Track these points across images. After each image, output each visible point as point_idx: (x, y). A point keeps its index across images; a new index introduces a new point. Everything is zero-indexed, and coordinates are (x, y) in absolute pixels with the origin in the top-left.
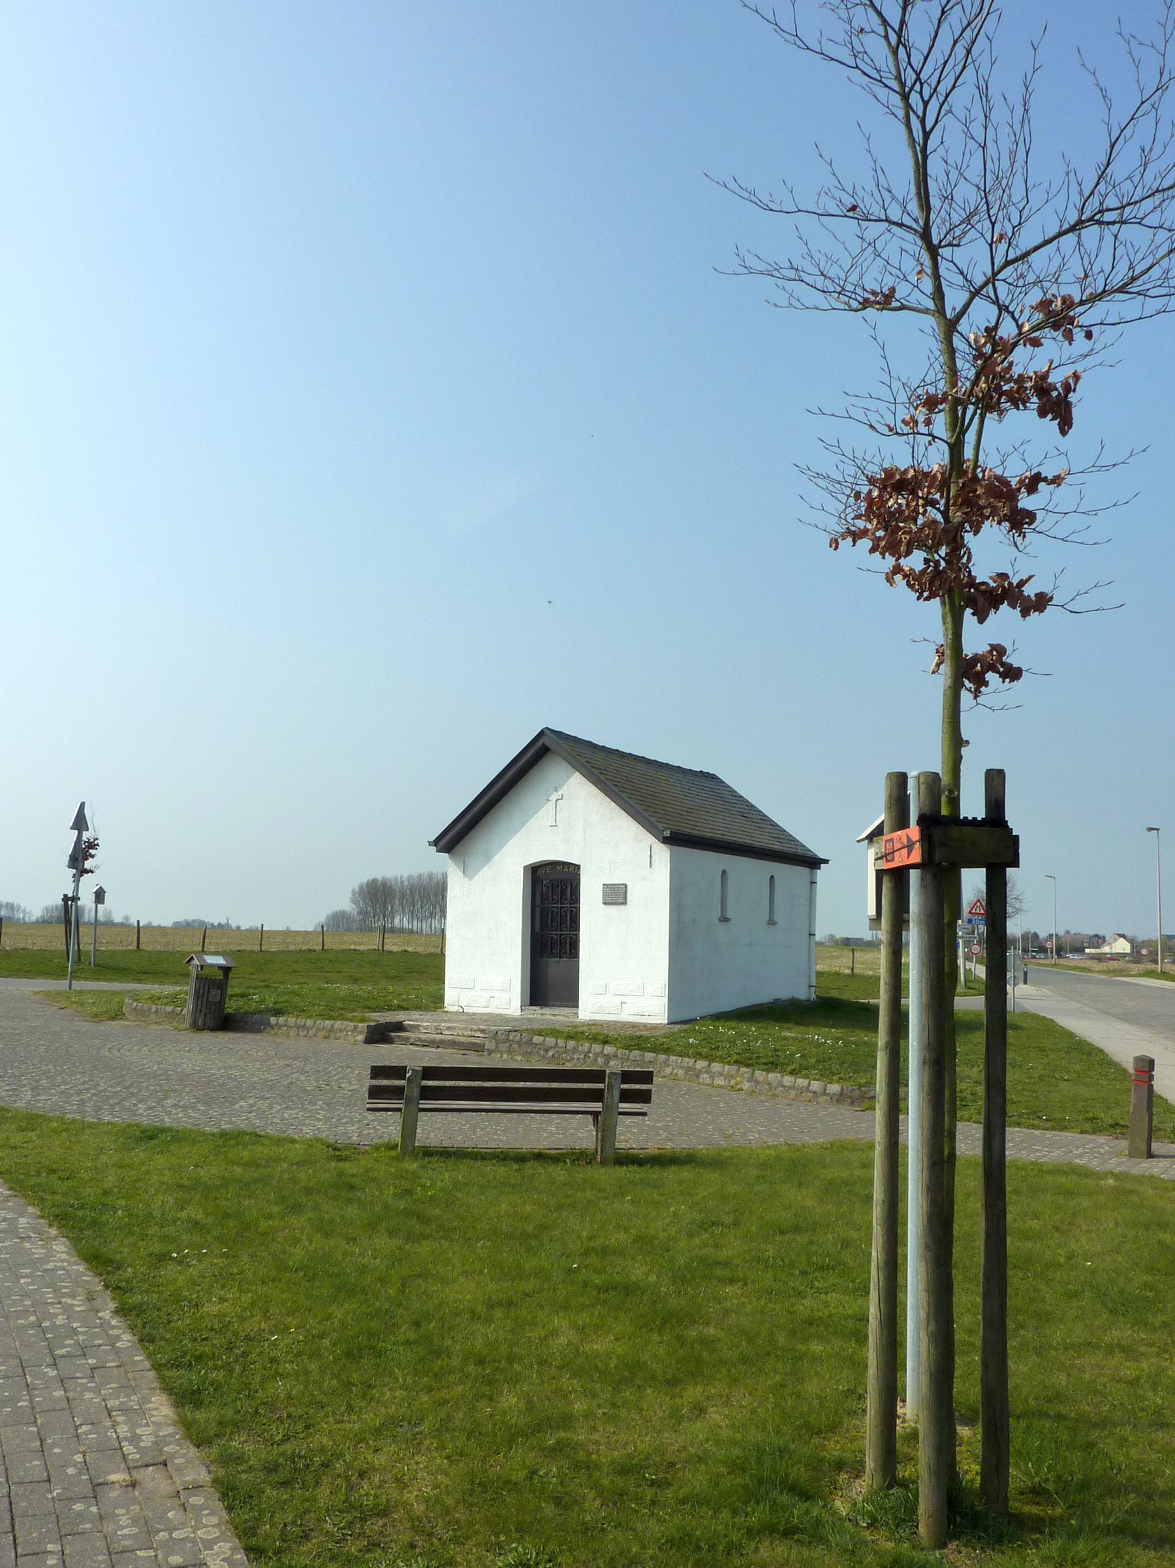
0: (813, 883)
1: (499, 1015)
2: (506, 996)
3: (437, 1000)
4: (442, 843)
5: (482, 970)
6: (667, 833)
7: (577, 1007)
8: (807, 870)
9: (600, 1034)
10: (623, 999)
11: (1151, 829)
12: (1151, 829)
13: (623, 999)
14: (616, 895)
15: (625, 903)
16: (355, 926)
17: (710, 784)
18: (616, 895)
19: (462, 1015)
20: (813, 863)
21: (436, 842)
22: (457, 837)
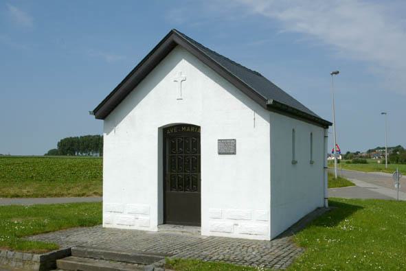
0: (326, 137)
1: (142, 231)
2: (147, 218)
3: (93, 219)
4: (98, 113)
5: (129, 194)
6: (270, 102)
7: (200, 225)
8: (322, 129)
9: (215, 242)
10: (236, 222)
11: (383, 113)
12: (383, 113)
13: (236, 222)
14: (227, 147)
15: (234, 153)
16: (59, 153)
17: (259, 77)
18: (227, 147)
19: (114, 232)
20: (326, 125)
21: (95, 112)
22: (110, 109)
